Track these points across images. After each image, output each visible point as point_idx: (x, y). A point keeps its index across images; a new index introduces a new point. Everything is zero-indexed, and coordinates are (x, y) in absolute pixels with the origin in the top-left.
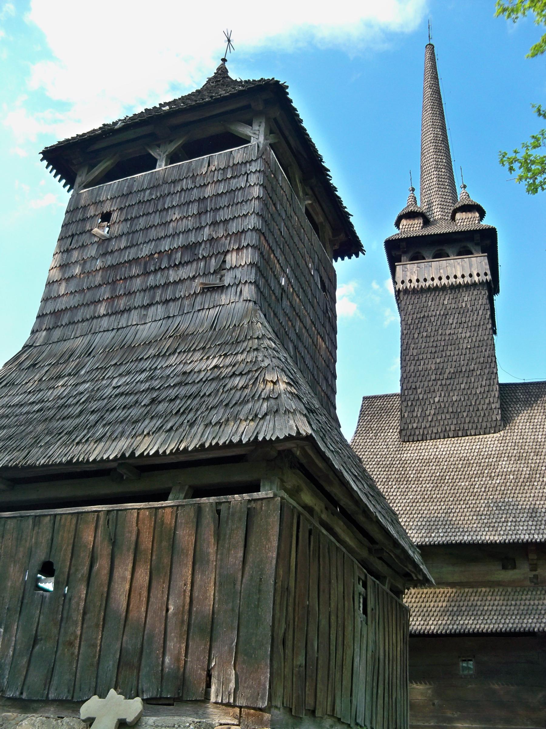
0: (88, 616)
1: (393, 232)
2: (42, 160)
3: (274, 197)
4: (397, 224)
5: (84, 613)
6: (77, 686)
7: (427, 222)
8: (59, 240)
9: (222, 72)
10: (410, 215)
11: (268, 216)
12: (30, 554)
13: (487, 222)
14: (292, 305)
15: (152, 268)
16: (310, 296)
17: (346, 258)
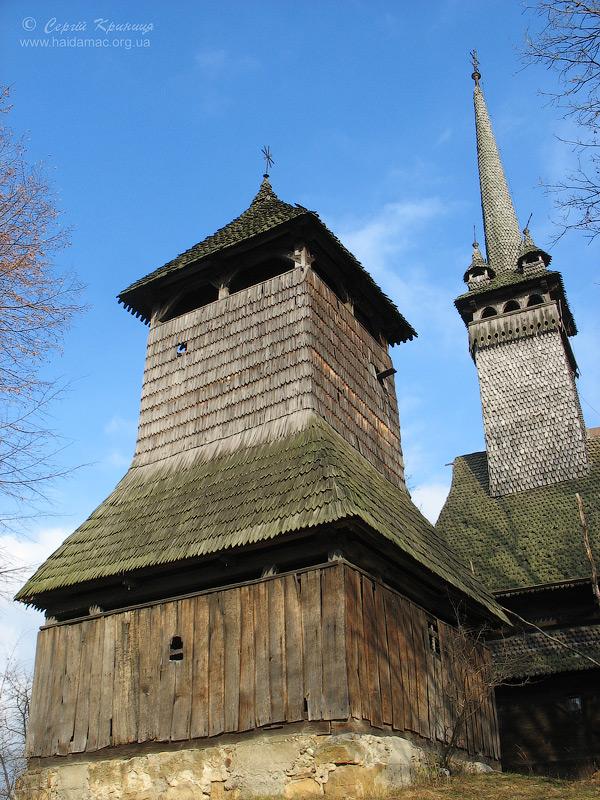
0: (212, 673)
1: (463, 290)
2: (119, 302)
3: (322, 314)
4: (466, 279)
5: (209, 671)
6: (211, 726)
7: (492, 274)
8: (467, 457)
9: (266, 189)
10: (476, 271)
11: (316, 332)
12: (162, 633)
13: (552, 267)
14: (349, 402)
15: (227, 389)
16: (366, 388)
17: (401, 342)
